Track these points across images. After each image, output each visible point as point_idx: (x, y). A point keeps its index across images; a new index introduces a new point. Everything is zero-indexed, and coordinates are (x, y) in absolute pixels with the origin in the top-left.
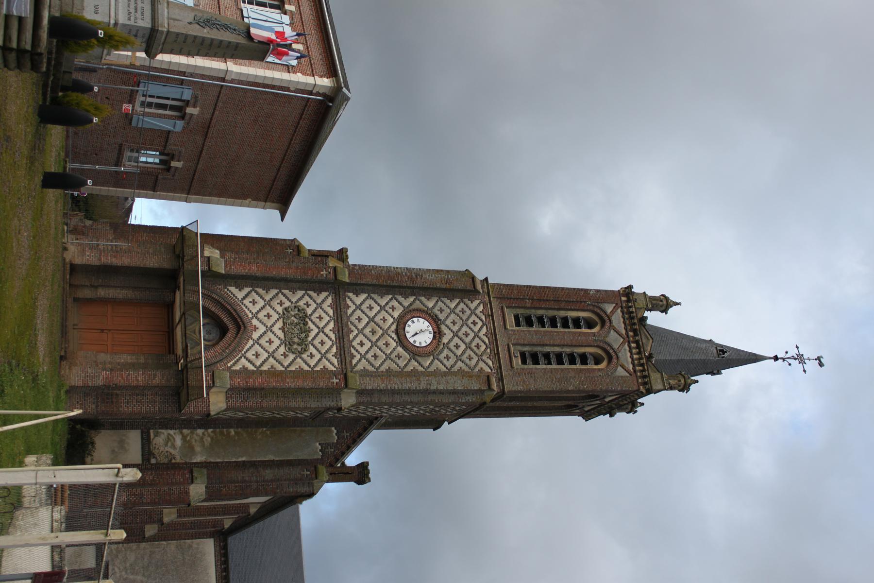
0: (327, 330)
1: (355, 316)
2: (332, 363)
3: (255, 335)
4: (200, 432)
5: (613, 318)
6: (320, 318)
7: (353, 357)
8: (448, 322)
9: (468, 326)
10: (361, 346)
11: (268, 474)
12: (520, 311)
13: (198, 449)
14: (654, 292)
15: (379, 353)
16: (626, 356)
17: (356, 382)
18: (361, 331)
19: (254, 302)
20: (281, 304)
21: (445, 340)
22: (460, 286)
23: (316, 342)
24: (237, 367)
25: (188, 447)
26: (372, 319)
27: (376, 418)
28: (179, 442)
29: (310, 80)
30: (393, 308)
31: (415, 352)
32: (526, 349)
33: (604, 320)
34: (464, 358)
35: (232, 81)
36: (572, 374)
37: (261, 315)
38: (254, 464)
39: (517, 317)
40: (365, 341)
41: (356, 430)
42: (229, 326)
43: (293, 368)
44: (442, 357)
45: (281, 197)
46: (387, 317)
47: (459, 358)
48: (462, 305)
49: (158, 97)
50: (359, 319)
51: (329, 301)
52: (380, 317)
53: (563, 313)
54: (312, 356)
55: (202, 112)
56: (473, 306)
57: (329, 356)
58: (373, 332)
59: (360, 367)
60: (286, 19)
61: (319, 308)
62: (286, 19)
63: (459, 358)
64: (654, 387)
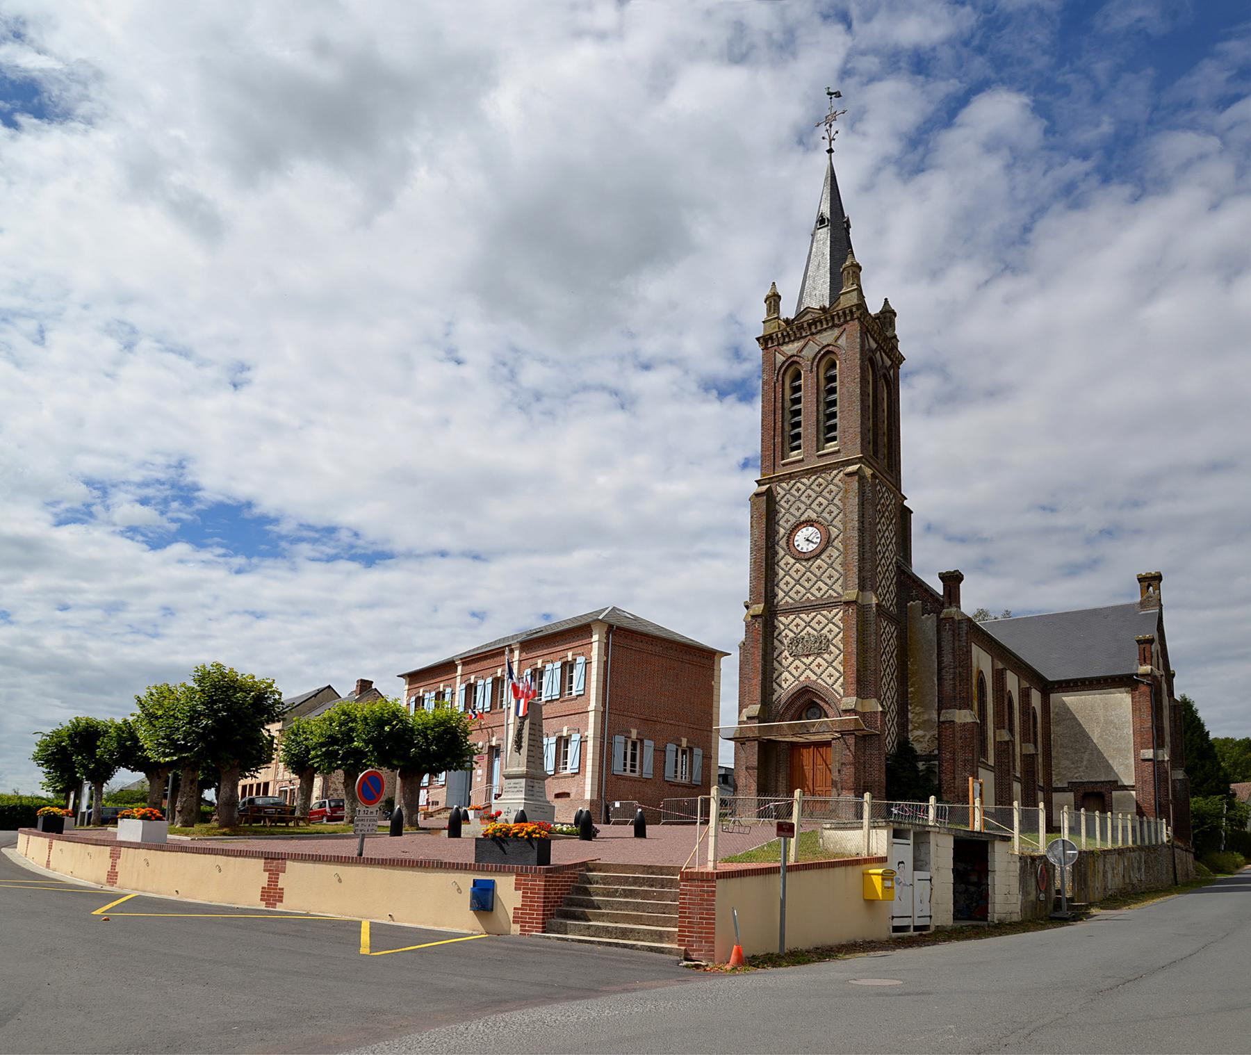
0: (808, 620)
1: (794, 596)
2: (837, 614)
3: (814, 677)
4: (910, 716)
5: (790, 354)
6: (797, 625)
7: (831, 596)
8: (798, 514)
9: (796, 500)
10: (819, 591)
11: (948, 659)
12: (787, 447)
13: (926, 717)
14: (762, 311)
15: (827, 574)
16: (827, 338)
17: (852, 594)
18: (808, 590)
19: (786, 680)
20: (786, 658)
21: (814, 516)
22: (767, 508)
23: (818, 628)
24: (841, 691)
25: (924, 725)
26: (797, 582)
27: (898, 567)
28: (920, 733)
29: (595, 645)
30: (787, 564)
31: (827, 542)
32: (822, 437)
33: (792, 362)
34: (830, 497)
35: (604, 707)
36: (844, 390)
37: (796, 674)
38: (940, 670)
39: (793, 449)
40: (816, 586)
41: (908, 584)
42: (808, 701)
43: (841, 646)
44: (830, 518)
45: (706, 658)
46: (794, 569)
47: (831, 502)
48: (782, 503)
49: (625, 759)
50: (798, 592)
51: (782, 619)
52: (794, 575)
53: (788, 404)
54: (830, 631)
55: (635, 727)
56: (782, 493)
57: (830, 616)
58: (808, 580)
59: (840, 590)
60: (549, 666)
61: (788, 626)
62: (549, 666)
63: (831, 502)
64: (855, 301)
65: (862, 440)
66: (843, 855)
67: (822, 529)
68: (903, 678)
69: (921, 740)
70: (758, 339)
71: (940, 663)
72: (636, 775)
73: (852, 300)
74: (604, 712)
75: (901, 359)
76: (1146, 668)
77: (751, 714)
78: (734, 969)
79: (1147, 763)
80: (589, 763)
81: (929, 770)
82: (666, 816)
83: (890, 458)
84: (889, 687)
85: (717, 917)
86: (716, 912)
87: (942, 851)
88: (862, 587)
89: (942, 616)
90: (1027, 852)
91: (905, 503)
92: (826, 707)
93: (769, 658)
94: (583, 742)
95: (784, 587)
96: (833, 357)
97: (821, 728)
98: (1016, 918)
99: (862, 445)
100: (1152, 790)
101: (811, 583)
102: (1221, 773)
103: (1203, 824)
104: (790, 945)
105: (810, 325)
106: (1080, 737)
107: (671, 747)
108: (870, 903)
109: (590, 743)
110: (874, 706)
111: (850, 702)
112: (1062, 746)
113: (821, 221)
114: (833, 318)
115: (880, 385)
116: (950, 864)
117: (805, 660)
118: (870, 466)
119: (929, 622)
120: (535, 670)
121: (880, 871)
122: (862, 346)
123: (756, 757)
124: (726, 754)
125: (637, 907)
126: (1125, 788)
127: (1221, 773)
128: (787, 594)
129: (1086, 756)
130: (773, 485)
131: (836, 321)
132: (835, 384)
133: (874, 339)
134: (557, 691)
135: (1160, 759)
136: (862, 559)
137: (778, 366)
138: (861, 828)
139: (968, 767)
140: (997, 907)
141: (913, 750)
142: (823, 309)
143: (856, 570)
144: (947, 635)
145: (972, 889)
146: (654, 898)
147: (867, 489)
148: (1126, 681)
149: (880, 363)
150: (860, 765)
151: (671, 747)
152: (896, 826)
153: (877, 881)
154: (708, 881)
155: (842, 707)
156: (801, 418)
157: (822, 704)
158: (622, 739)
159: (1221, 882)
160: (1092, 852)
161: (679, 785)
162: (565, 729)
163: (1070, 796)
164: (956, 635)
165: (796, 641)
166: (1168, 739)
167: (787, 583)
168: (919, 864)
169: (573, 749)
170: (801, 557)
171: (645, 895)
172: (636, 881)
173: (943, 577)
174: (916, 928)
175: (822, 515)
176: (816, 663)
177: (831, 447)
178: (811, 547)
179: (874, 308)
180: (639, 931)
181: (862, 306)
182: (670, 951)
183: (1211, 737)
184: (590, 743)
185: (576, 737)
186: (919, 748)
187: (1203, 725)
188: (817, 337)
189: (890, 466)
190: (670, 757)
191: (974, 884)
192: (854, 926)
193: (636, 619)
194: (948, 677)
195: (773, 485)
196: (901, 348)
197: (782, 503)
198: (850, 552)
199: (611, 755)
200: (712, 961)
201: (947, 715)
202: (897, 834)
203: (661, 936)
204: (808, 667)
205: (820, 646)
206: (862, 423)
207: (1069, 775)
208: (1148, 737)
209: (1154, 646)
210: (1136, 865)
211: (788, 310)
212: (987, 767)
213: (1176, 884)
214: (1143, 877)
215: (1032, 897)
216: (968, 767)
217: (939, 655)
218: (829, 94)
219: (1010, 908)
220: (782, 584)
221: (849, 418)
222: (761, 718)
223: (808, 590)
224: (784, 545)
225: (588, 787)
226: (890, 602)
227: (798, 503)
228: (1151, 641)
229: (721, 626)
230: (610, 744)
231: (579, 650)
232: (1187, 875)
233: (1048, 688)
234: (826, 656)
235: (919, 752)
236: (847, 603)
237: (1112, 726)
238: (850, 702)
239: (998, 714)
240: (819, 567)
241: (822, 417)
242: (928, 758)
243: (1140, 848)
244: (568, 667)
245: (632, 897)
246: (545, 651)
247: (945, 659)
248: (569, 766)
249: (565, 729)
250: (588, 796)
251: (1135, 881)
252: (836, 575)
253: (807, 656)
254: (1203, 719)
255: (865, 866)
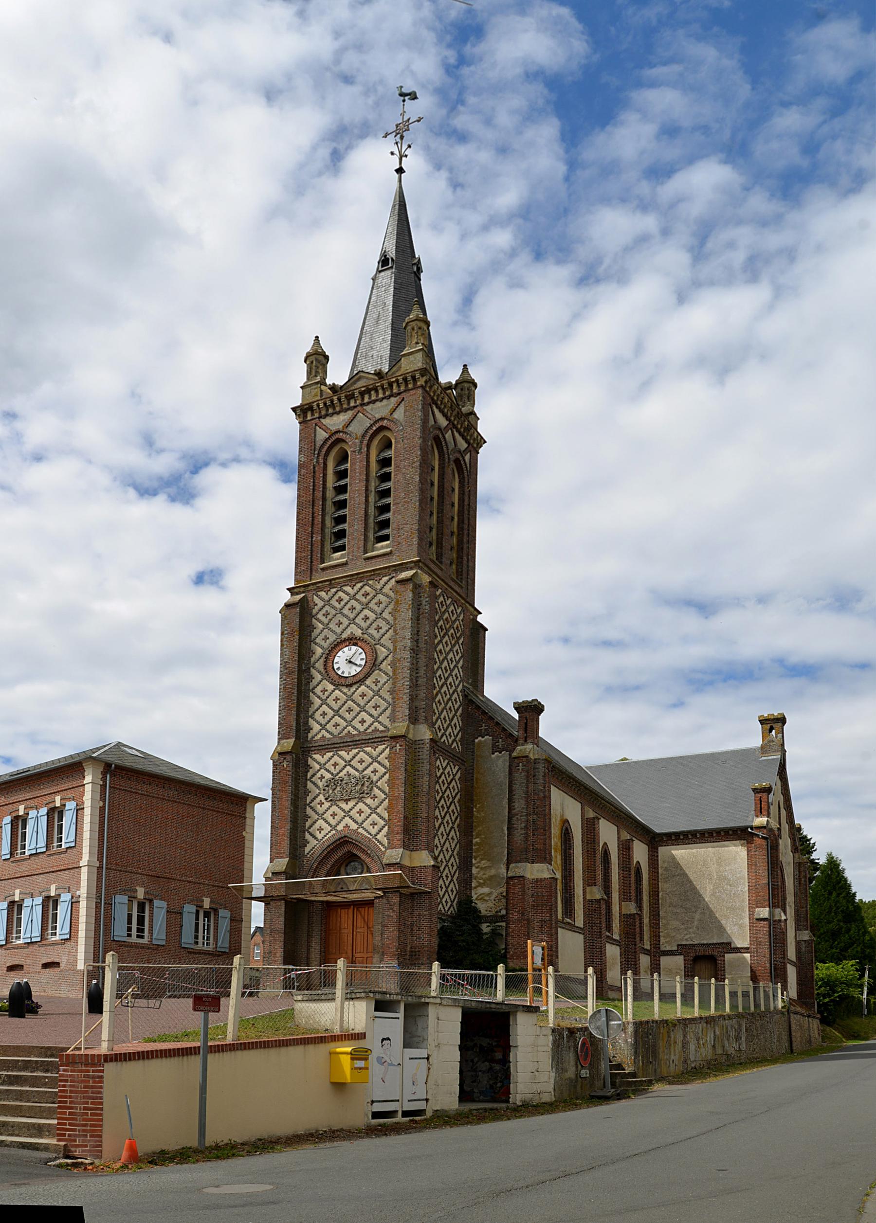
0: (348, 758)
1: (333, 730)
2: (383, 751)
3: (354, 826)
4: (474, 871)
5: (334, 429)
6: (335, 765)
7: (376, 730)
8: (338, 630)
9: (333, 613)
11: (520, 805)
12: (328, 547)
13: (493, 872)
14: (300, 374)
15: (372, 703)
16: (380, 410)
17: (401, 727)
18: (349, 723)
19: (320, 829)
20: (321, 804)
21: (358, 633)
22: (299, 620)
25: (490, 881)
26: (337, 712)
28: (486, 890)
29: (88, 788)
31: (373, 664)
32: (371, 536)
33: (336, 440)
34: (378, 610)
35: (101, 861)
36: (400, 477)
39: (336, 550)
40: (359, 718)
41: (478, 713)
42: (346, 853)
44: (377, 636)
45: (238, 803)
46: (333, 696)
50: (336, 725)
53: (330, 493)
54: (375, 771)
56: (320, 603)
58: (350, 710)
59: (387, 722)
60: (32, 813)
61: (324, 766)
62: (32, 813)
65: (421, 539)
66: (318, 1031)
67: (367, 648)
68: (467, 826)
69: (486, 898)
70: (294, 409)
71: (510, 809)
72: (145, 941)
73: (416, 362)
74: (100, 868)
75: (481, 441)
76: (762, 820)
77: (277, 869)
78: (125, 1167)
79: (762, 923)
80: (82, 927)
81: (495, 933)
82: (174, 988)
83: (460, 562)
84: (447, 839)
85: (105, 1106)
86: (105, 1100)
87: (445, 1027)
88: (414, 719)
89: (515, 754)
90: (566, 1024)
91: (480, 619)
92: (368, 860)
93: (300, 804)
94: (74, 903)
95: (320, 719)
96: (388, 434)
97: (358, 884)
98: (547, 1098)
99: (419, 545)
100: (767, 952)
101: (353, 714)
102: (867, 938)
103: (834, 992)
104: (211, 1139)
105: (362, 394)
106: (690, 894)
107: (189, 909)
108: (339, 1087)
109: (83, 904)
110: (424, 859)
111: (395, 854)
112: (671, 905)
113: (384, 261)
114: (391, 385)
115: (448, 471)
116: (456, 1039)
117: (343, 805)
118: (430, 572)
119: (500, 761)
120: (17, 818)
121: (349, 1049)
122: (425, 421)
123: (282, 919)
124: (257, 914)
125: (20, 1096)
126: (738, 950)
127: (867, 938)
128: (323, 727)
129: (697, 916)
130: (310, 595)
131: (395, 390)
132: (390, 471)
133: (445, 415)
134: (42, 843)
135: (777, 918)
136: (414, 685)
137: (319, 443)
138: (334, 999)
139: (546, 929)
140: (521, 1087)
141: (476, 911)
142: (379, 374)
143: (406, 698)
144: (520, 777)
145: (497, 1067)
146: (45, 1085)
147: (424, 601)
148: (741, 834)
149: (451, 445)
150: (405, 928)
151: (189, 909)
152: (378, 996)
153: (346, 1060)
154: (93, 1065)
155: (385, 861)
156: (346, 511)
157: (363, 857)
158: (124, 899)
159: (855, 1048)
160: (666, 1022)
161: (200, 952)
162: (53, 888)
163: (680, 960)
164: (530, 776)
165: (334, 783)
166: (790, 899)
167: (324, 714)
168: (411, 1039)
169: (63, 910)
170: (341, 682)
171: (35, 1082)
172: (27, 1065)
173: (518, 707)
174: (405, 1114)
175: (368, 627)
176: (357, 809)
177: (383, 547)
178: (354, 670)
179: (448, 375)
180: (13, 1125)
181: (430, 370)
182: (46, 1148)
183: (858, 898)
184: (83, 904)
185: (66, 897)
186: (483, 908)
187: (850, 886)
188: (368, 408)
189: (459, 573)
190: (188, 921)
191: (498, 1062)
192: (319, 1112)
193: (146, 756)
194: (519, 825)
195: (310, 595)
196: (482, 428)
197: (320, 616)
198: (400, 676)
199: (109, 920)
200: (100, 1157)
201: (518, 869)
202: (382, 1006)
203: (39, 1130)
204: (347, 813)
205: (361, 789)
206: (421, 519)
207: (679, 937)
208: (764, 894)
209: (775, 793)
210: (732, 1034)
211: (338, 374)
212: (572, 928)
213: (792, 1051)
214: (744, 1047)
215: (571, 1073)
216: (546, 929)
217: (510, 800)
218: (401, 95)
219: (539, 1088)
220: (317, 716)
221: (405, 514)
222: (288, 874)
223: (349, 723)
224: (322, 669)
225: (81, 956)
226: (452, 736)
227: (339, 617)
228: (768, 790)
229: (248, 770)
230: (109, 904)
231: (69, 794)
232: (810, 1042)
233: (655, 840)
234: (369, 801)
235: (483, 913)
236: (394, 738)
237: (725, 882)
238: (395, 854)
239: (589, 869)
240: (363, 695)
241: (372, 510)
242: (494, 919)
243: (739, 1016)
244: (55, 814)
245: (18, 1084)
246: (28, 795)
247: (516, 805)
248: (58, 931)
249: (53, 888)
250: (81, 966)
251: (731, 1051)
252: (384, 704)
253: (347, 801)
254: (849, 879)
255: (332, 1044)
